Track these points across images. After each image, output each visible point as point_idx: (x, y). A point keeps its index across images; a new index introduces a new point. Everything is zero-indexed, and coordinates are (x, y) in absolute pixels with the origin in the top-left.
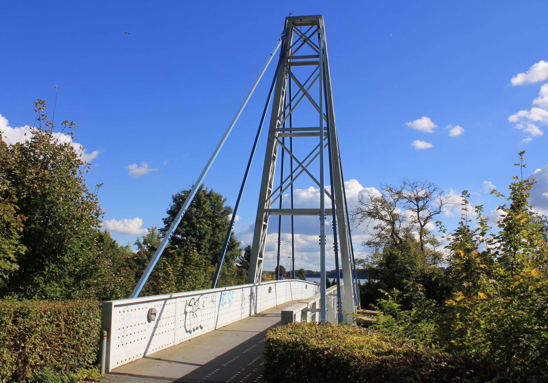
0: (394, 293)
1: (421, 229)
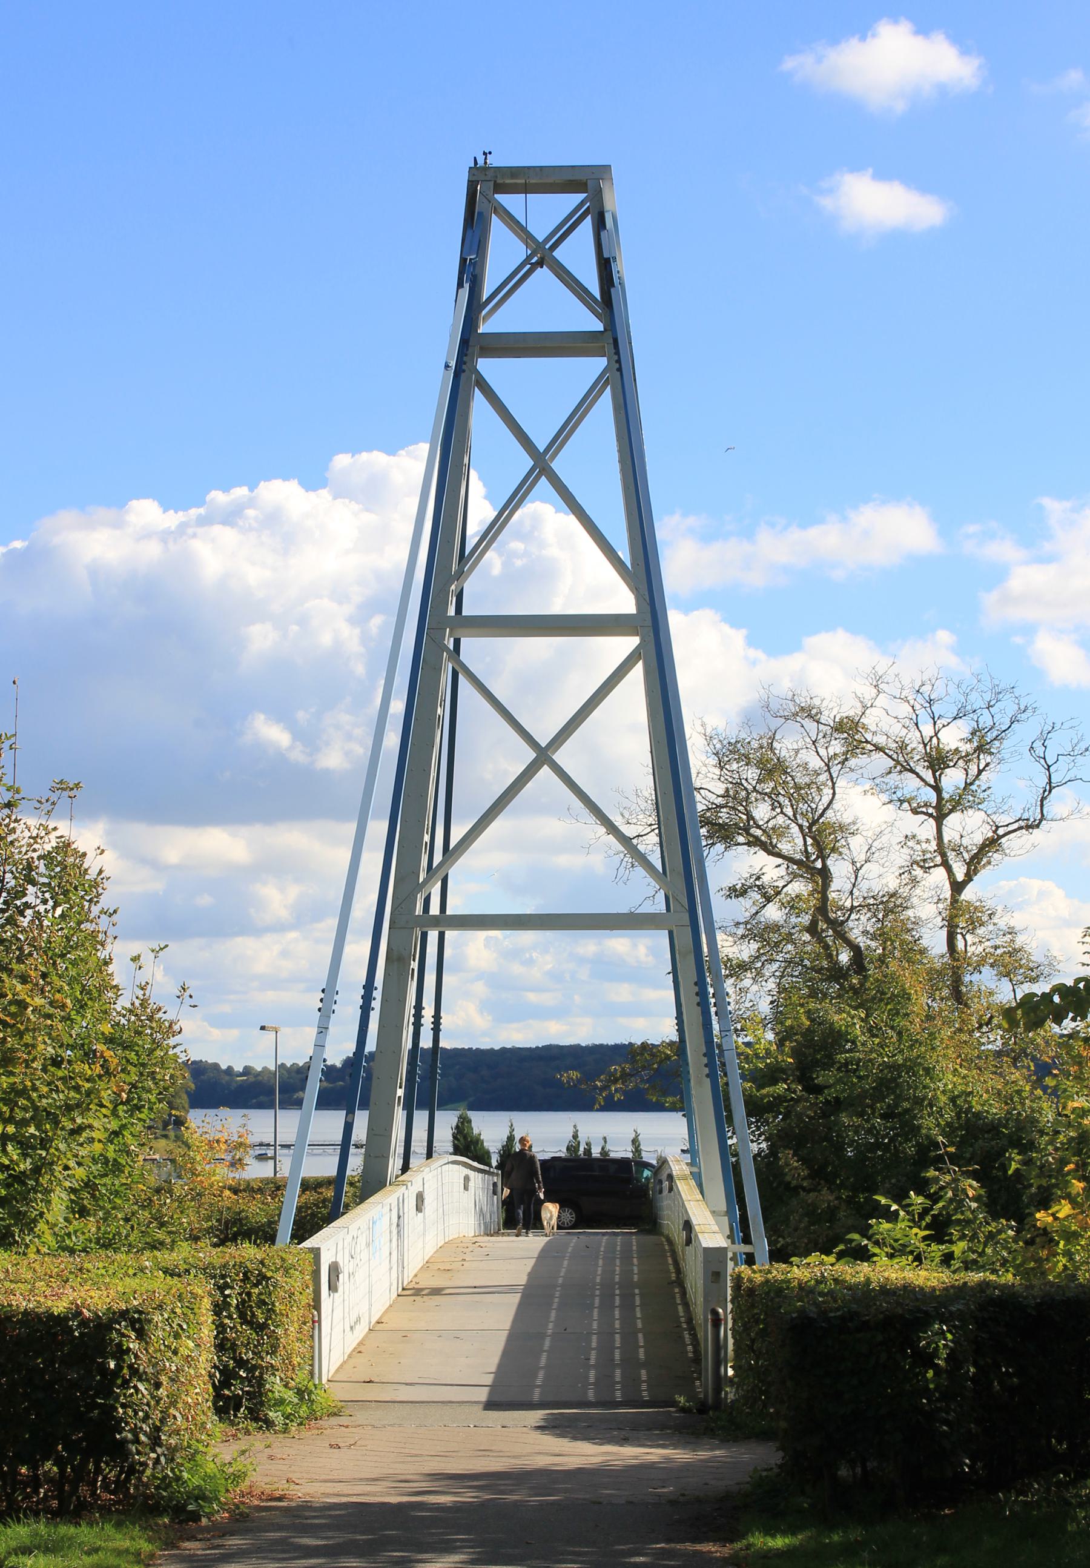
0: (912, 1205)
1: (954, 901)
